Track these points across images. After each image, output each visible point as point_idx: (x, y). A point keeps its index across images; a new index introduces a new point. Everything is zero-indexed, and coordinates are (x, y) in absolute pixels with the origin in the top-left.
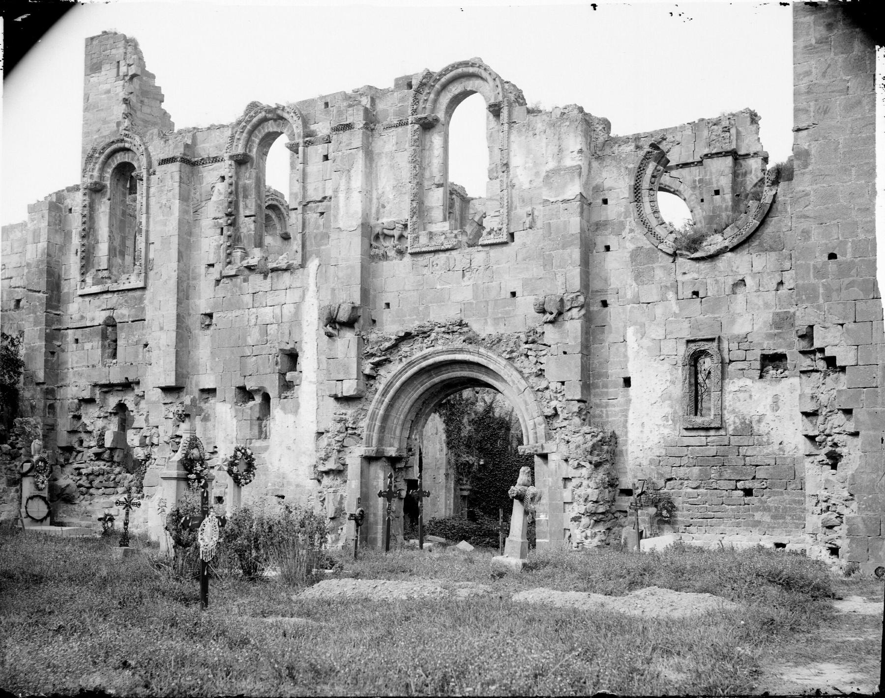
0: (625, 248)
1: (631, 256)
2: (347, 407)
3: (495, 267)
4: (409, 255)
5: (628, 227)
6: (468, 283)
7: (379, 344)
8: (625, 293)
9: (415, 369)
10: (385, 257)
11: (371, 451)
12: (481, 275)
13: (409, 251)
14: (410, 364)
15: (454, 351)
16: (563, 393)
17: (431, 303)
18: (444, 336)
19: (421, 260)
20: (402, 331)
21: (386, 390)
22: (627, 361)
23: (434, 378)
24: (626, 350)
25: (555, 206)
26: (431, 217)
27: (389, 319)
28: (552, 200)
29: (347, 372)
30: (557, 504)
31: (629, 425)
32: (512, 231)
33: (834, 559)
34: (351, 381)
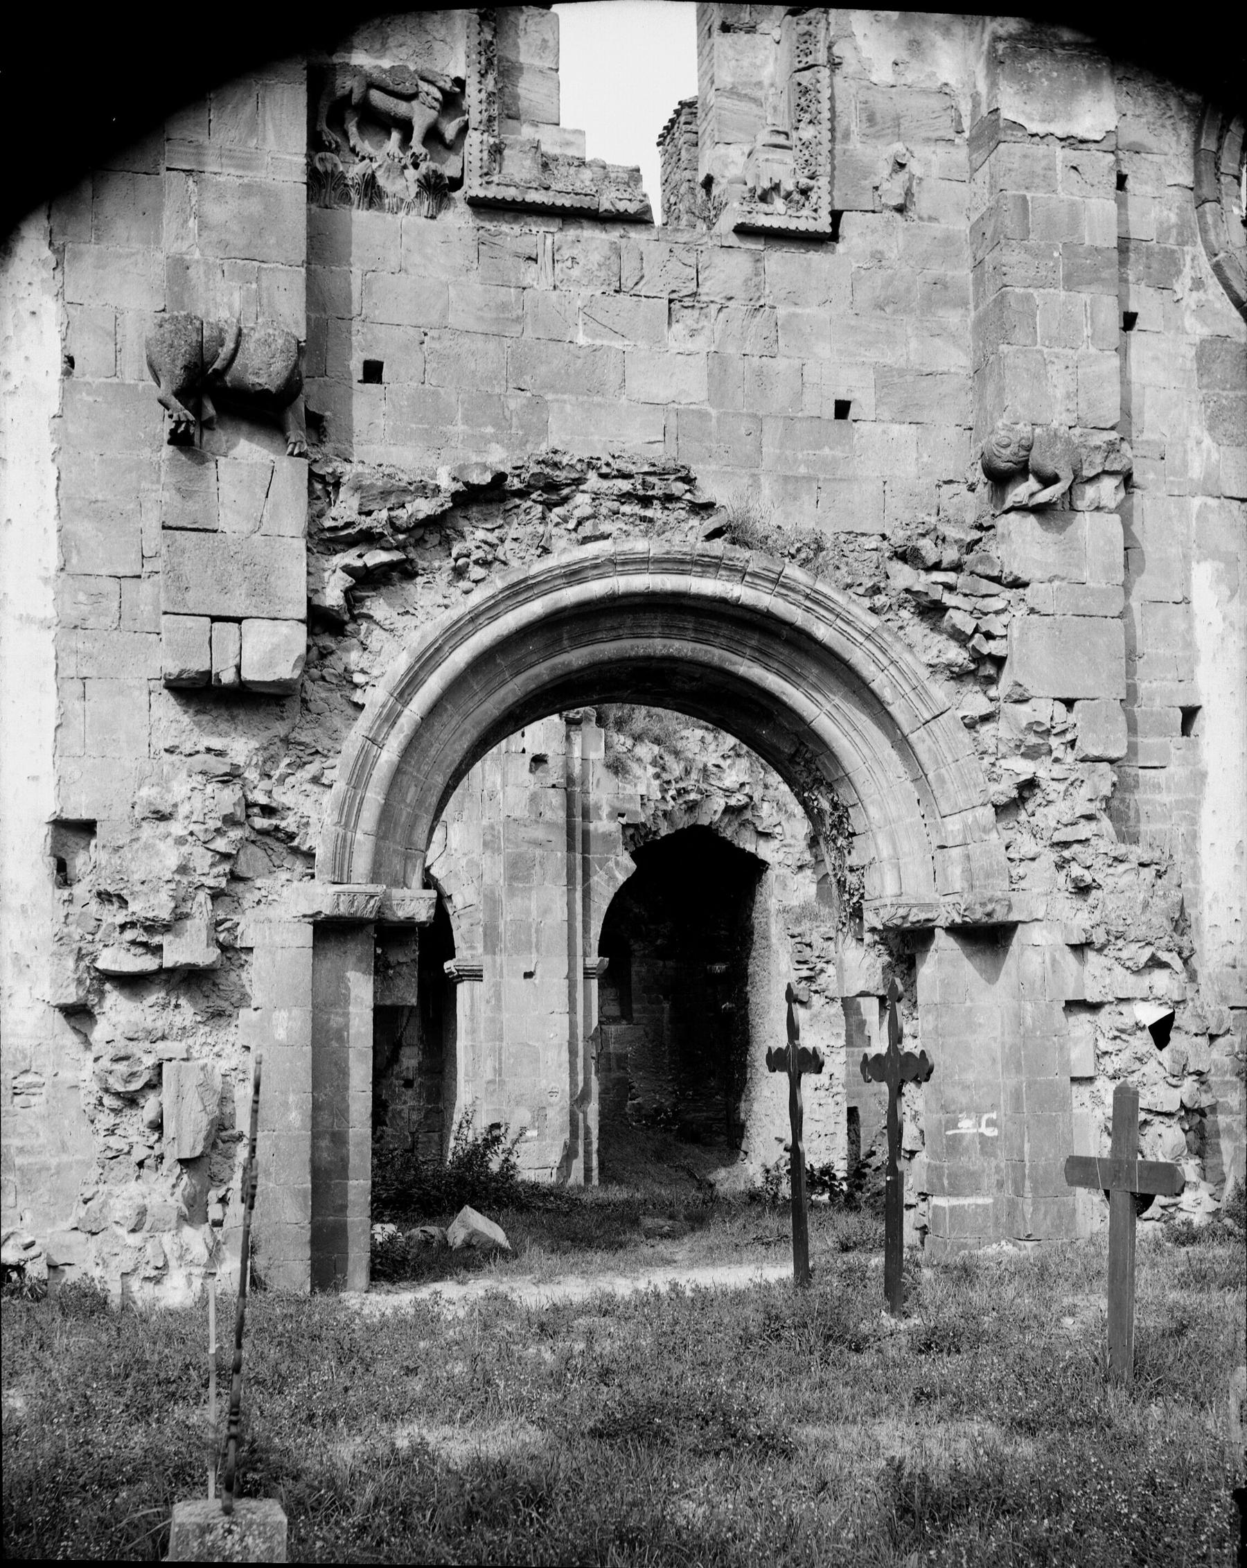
0: (1181, 330)
1: (1199, 357)
2: (223, 726)
3: (782, 312)
4: (463, 207)
5: (1188, 272)
6: (690, 346)
7: (393, 500)
8: (1185, 464)
9: (536, 608)
10: (371, 192)
11: (361, 900)
12: (735, 326)
13: (474, 187)
14: (519, 591)
15: (679, 564)
16: (1069, 737)
17: (552, 387)
18: (626, 509)
19: (510, 232)
20: (485, 467)
21: (416, 674)
22: (1191, 661)
23: (563, 651)
24: (1190, 628)
25: (1042, 149)
26: (516, 97)
27: (381, 422)
28: (1033, 127)
29: (261, 588)
30: (1051, 1084)
31: (1203, 847)
32: (838, 207)
33: (167, 1155)
34: (283, 628)
